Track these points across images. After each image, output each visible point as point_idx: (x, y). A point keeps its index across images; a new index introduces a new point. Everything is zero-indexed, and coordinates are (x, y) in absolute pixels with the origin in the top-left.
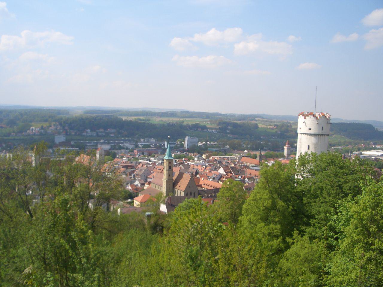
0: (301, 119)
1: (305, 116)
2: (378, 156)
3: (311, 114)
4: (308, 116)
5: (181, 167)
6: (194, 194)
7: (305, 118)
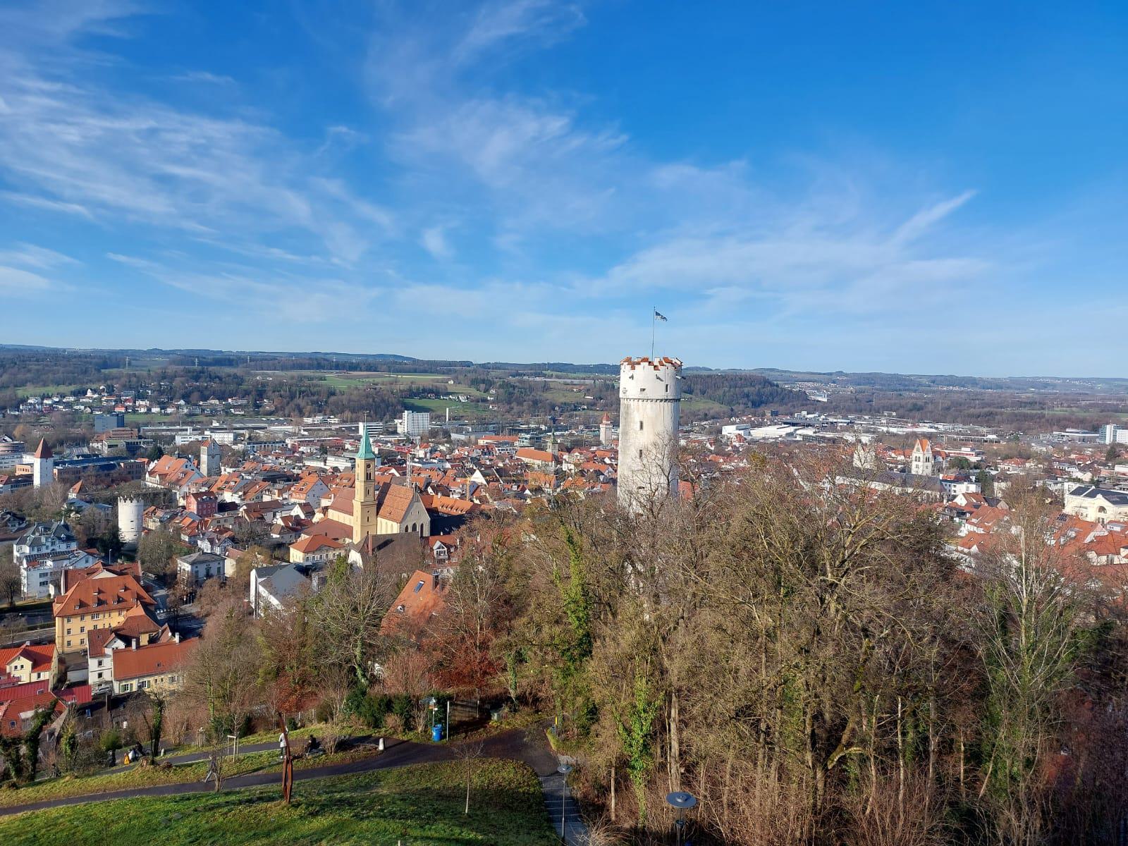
0: (626, 371)
1: (633, 365)
2: (781, 436)
3: (645, 360)
4: (639, 363)
5: (393, 474)
6: (422, 526)
7: (633, 368)
